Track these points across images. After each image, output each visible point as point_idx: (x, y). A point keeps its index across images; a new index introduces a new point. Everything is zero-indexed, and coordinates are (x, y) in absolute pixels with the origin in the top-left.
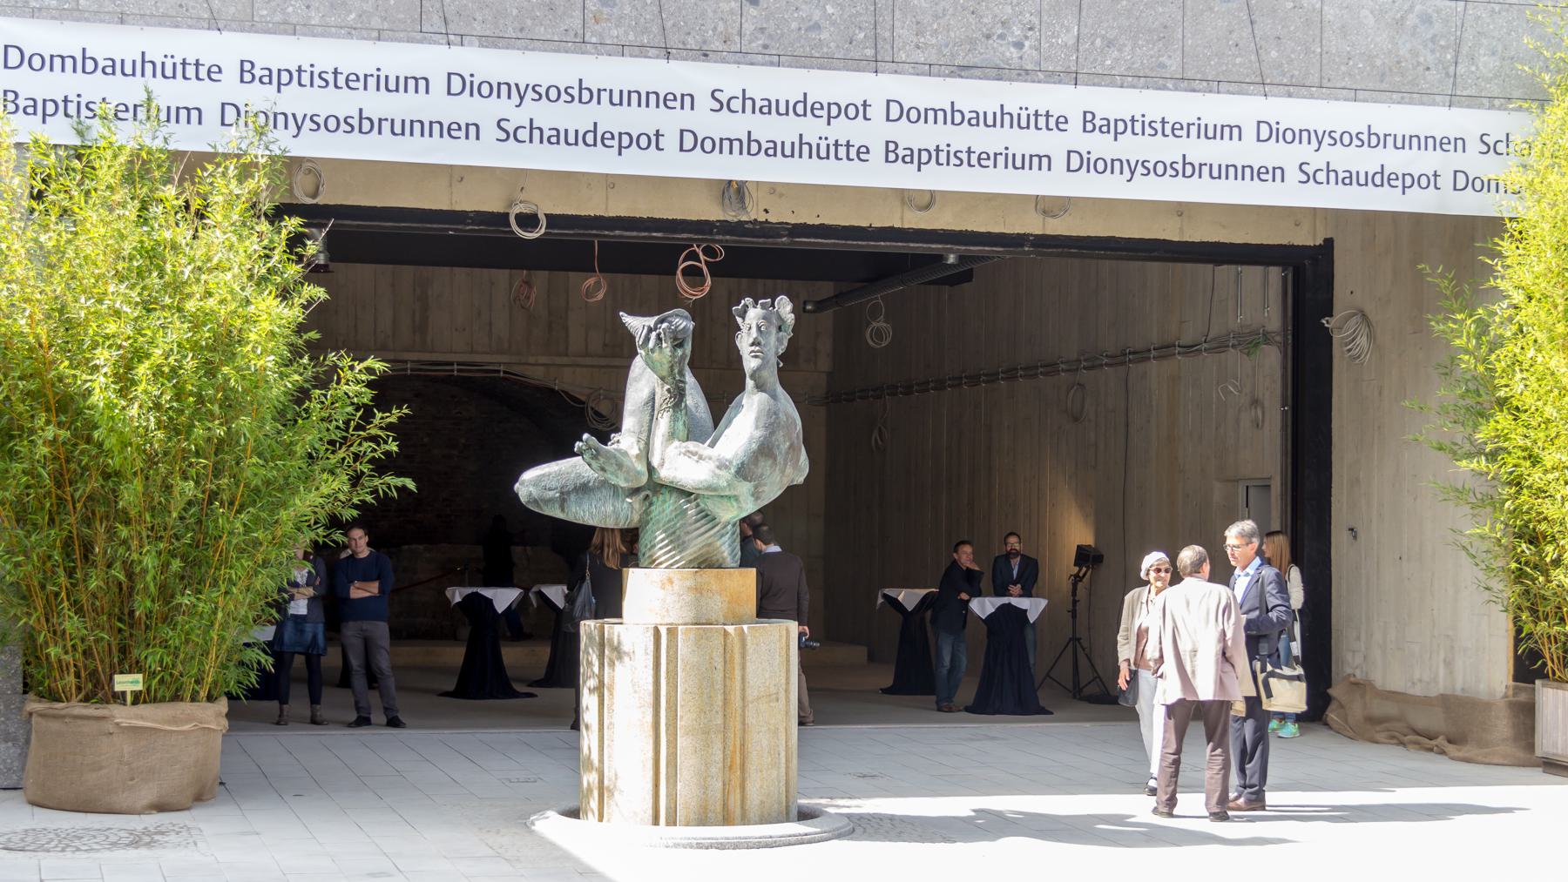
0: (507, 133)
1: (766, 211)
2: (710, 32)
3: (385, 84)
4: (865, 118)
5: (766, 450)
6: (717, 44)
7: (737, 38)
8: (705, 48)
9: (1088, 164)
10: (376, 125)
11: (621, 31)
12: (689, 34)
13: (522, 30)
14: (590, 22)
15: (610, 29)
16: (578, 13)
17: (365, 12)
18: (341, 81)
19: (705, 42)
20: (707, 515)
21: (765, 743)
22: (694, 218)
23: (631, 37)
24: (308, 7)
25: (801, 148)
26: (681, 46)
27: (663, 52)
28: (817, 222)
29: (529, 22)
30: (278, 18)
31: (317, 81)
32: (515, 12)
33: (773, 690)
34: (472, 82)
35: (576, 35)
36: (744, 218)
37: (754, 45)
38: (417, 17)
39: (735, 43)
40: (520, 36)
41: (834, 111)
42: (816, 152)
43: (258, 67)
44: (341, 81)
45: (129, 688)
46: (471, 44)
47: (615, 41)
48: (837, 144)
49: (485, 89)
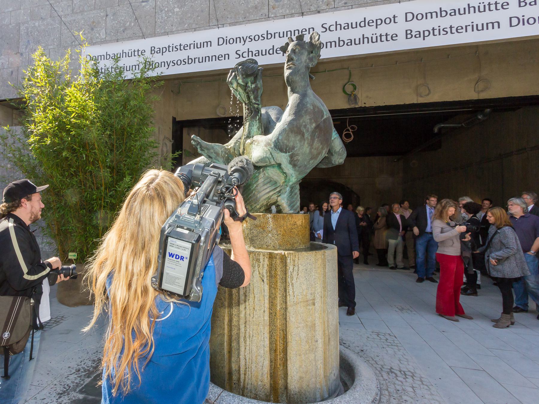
0: (239, 55)
1: (365, 103)
2: (321, 3)
3: (197, 46)
4: (395, 22)
5: (295, 129)
6: (324, 6)
7: (333, 3)
8: (319, 9)
9: (522, 21)
10: (193, 60)
11: (283, 10)
12: (312, 5)
13: (245, 18)
14: (271, 9)
15: (279, 10)
16: (266, 7)
17: (190, 23)
18: (454, 30)
19: (318, 7)
20: (271, 181)
21: (303, 335)
22: (339, 108)
23: (288, 12)
24: (172, 26)
25: (364, 39)
26: (308, 11)
27: (301, 14)
28: (384, 105)
29: (248, 14)
30: (163, 31)
31: (442, 32)
32: (242, 12)
33: (309, 297)
34: (523, 19)
35: (265, 15)
36: (357, 106)
37: (340, 4)
38: (208, 21)
39: (332, 5)
40: (244, 20)
41: (378, 23)
42: (371, 40)
43: (156, 48)
44: (454, 30)
45: (73, 258)
46: (226, 26)
47: (281, 14)
48: (381, 36)
49: (531, 21)
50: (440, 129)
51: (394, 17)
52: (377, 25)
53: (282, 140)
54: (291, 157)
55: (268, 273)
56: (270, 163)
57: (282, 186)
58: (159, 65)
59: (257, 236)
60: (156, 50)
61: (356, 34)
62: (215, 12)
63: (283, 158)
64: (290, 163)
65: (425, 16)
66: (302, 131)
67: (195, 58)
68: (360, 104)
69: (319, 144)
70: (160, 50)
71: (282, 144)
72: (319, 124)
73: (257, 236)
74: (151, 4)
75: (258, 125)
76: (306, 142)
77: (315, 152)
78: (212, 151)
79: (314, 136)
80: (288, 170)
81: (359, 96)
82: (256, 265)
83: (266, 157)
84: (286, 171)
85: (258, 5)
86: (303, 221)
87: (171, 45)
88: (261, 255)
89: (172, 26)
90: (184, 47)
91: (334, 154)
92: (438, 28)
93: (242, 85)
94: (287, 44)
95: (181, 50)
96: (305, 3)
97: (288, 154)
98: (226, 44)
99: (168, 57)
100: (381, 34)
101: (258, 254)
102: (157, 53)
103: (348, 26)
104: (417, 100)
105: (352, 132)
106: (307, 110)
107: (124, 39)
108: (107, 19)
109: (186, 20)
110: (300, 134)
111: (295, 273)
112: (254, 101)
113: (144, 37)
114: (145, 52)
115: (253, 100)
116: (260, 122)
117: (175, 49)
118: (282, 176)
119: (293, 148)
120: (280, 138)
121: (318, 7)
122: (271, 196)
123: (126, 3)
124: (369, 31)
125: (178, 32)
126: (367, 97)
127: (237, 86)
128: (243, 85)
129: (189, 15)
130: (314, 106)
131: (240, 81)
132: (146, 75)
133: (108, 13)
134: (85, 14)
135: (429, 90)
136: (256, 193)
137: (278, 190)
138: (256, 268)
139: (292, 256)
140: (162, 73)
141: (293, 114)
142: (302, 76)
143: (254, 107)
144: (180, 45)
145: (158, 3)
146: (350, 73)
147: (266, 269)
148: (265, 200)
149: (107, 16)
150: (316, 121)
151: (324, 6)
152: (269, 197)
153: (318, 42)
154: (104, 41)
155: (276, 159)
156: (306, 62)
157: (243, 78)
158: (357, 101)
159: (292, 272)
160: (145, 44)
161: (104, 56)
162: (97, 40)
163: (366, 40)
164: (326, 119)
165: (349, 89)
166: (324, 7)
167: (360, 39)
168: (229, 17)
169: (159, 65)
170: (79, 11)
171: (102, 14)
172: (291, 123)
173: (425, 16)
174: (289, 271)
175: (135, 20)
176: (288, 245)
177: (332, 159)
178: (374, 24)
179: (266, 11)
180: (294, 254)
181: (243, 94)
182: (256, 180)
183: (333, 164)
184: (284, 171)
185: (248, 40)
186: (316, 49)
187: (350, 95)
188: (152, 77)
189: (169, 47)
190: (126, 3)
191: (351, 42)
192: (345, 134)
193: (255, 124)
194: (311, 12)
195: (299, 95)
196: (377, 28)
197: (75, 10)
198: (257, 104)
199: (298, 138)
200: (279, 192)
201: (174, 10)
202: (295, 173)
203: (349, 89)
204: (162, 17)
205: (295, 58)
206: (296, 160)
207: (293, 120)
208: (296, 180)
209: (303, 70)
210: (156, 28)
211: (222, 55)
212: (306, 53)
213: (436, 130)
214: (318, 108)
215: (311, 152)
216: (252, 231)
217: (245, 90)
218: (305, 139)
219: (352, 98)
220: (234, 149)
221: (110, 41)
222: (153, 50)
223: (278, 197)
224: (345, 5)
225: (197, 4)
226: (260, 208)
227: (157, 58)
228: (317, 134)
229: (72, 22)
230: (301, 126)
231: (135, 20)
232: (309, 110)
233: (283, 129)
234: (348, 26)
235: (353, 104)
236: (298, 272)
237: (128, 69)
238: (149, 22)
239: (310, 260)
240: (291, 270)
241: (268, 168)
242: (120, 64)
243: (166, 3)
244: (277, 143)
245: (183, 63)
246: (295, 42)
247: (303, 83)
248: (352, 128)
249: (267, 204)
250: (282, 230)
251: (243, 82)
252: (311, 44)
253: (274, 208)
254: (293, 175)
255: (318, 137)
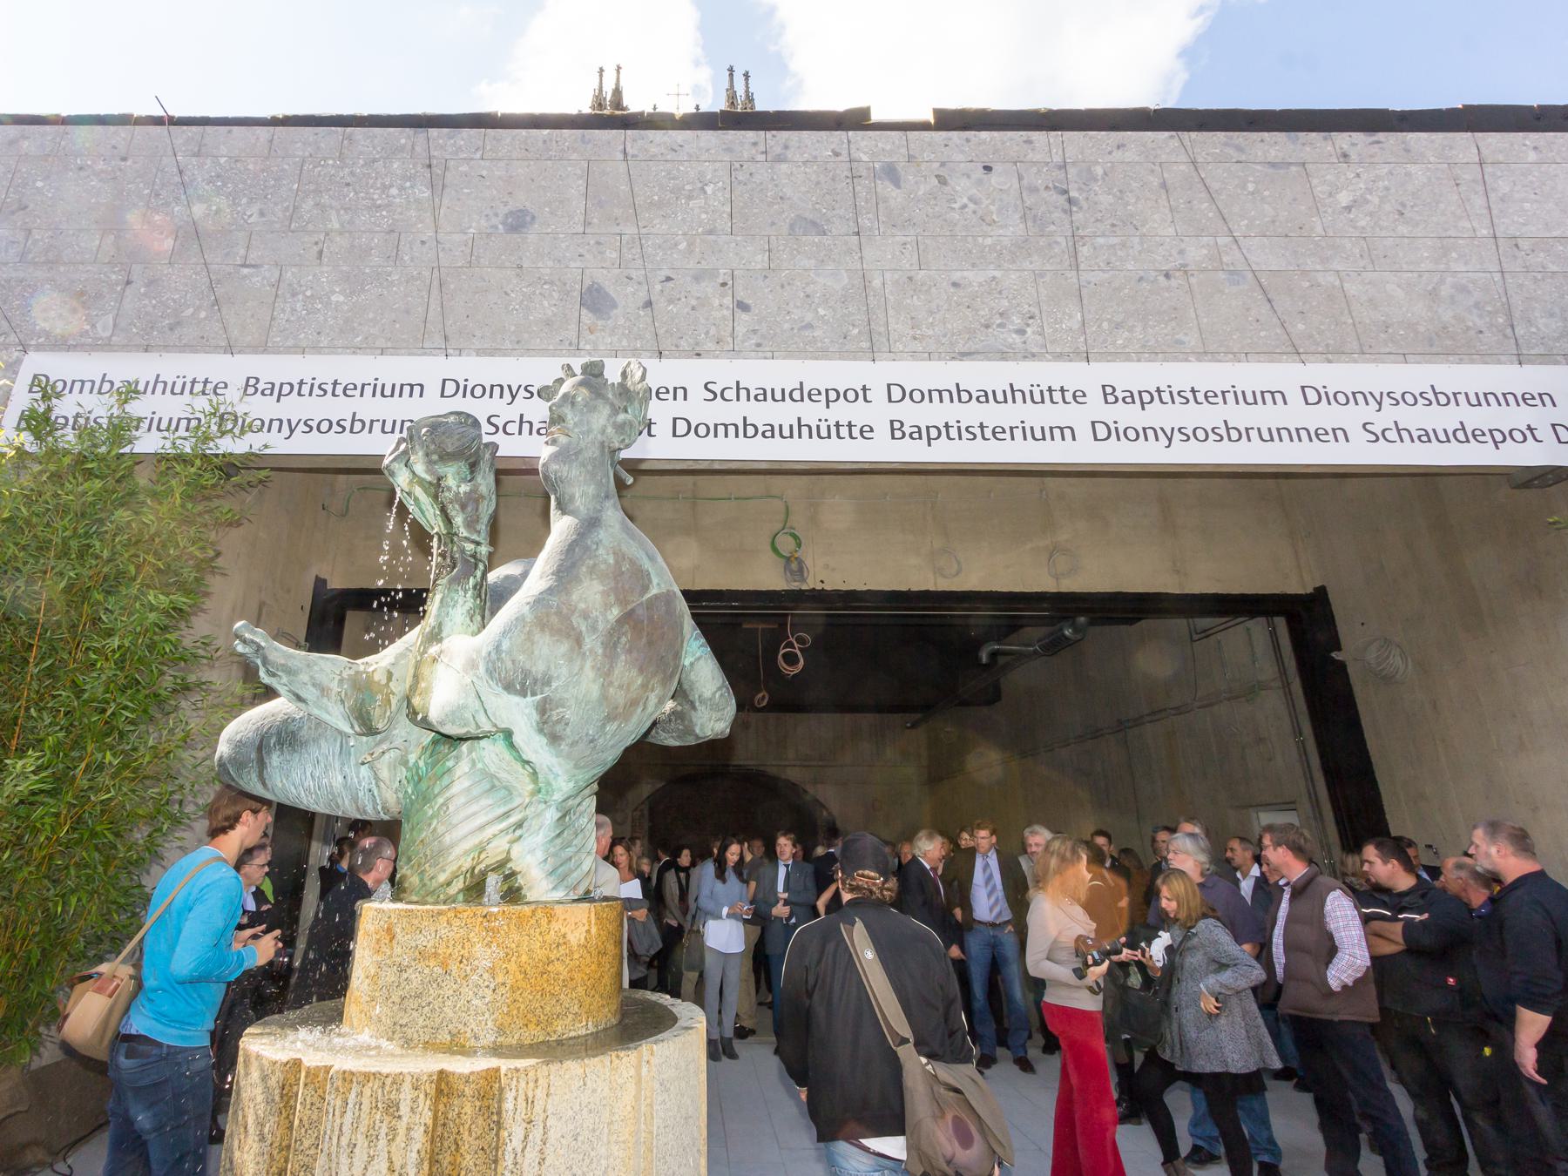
1: (822, 582)
3: (379, 391)
5: (554, 620)
9: (1115, 432)
11: (615, 339)
14: (585, 333)
19: (697, 344)
24: (319, 333)
25: (799, 428)
26: (674, 348)
27: (658, 354)
30: (290, 343)
32: (513, 328)
35: (570, 344)
36: (804, 587)
41: (831, 396)
42: (815, 432)
46: (468, 355)
50: (994, 655)
51: (864, 389)
52: (828, 401)
53: (509, 652)
54: (543, 709)
55: (426, 1166)
56: (478, 726)
57: (530, 803)
58: (264, 426)
59: (418, 996)
60: (261, 386)
61: (784, 414)
62: (441, 318)
63: (518, 713)
64: (541, 731)
65: (927, 396)
66: (574, 629)
67: (372, 421)
68: (811, 583)
69: (634, 672)
70: (272, 389)
71: (509, 665)
72: (633, 610)
73: (418, 996)
74: (267, 274)
75: (470, 604)
76: (588, 664)
77: (620, 698)
78: (304, 677)
79: (615, 646)
80: (536, 752)
81: (808, 562)
82: (384, 1130)
83: (464, 707)
84: (528, 755)
85: (554, 319)
86: (594, 930)
87: (308, 380)
88: (407, 1086)
89: (319, 333)
90: (335, 389)
91: (697, 704)
92: (956, 425)
93: (423, 479)
94: (560, 381)
95: (334, 395)
96: (667, 331)
97: (529, 699)
98: (464, 396)
99: (293, 408)
100: (837, 422)
101: (394, 1082)
102: (263, 394)
103: (763, 395)
104: (935, 584)
105: (800, 649)
106: (595, 565)
107: (167, 348)
108: (128, 292)
109: (360, 324)
110: (568, 636)
111: (531, 1155)
112: (463, 532)
113: (230, 349)
114: (226, 387)
115: (462, 529)
116: (480, 596)
117: (316, 391)
118: (521, 770)
119: (547, 681)
120: (505, 645)
121: (697, 344)
122: (489, 842)
123: (194, 260)
124: (811, 412)
125: (332, 349)
126: (827, 566)
127: (411, 482)
128: (430, 483)
129: (371, 315)
130: (620, 556)
131: (420, 469)
132: (211, 449)
133: (134, 278)
134: (62, 269)
135: (959, 563)
136: (441, 829)
137: (513, 819)
138: (382, 1143)
139: (523, 1084)
140: (266, 446)
141: (553, 574)
142: (590, 468)
143: (463, 551)
144: (335, 383)
145: (289, 274)
146: (787, 508)
147: (418, 1146)
148: (467, 853)
149: (128, 283)
150: (622, 602)
151: (710, 344)
152: (481, 843)
153: (640, 386)
154: (106, 345)
155: (494, 714)
156: (603, 432)
157: (430, 463)
158: (805, 575)
159: (519, 1150)
160: (230, 369)
161: (93, 382)
162: (83, 340)
163: (805, 430)
164: (656, 597)
165: (786, 544)
166: (710, 346)
167: (791, 426)
168: (479, 334)
169: (264, 426)
170: (43, 259)
171: (114, 277)
172: (539, 602)
173: (927, 396)
174: (509, 1148)
175: (213, 305)
176: (532, 1026)
177: (694, 720)
178: (823, 398)
179: (573, 335)
180: (531, 1074)
181: (430, 508)
182: (446, 780)
183: (697, 737)
184: (525, 757)
185: (522, 393)
186: (636, 404)
187: (788, 560)
188: (231, 454)
189: (301, 383)
190: (194, 260)
191: (771, 432)
192: (784, 655)
193: (461, 601)
194: (680, 353)
195: (577, 521)
196: (828, 407)
197: (30, 256)
198: (473, 542)
199: (564, 647)
200: (519, 825)
201: (329, 298)
202: (560, 764)
203: (786, 544)
204: (293, 310)
205: (569, 417)
206: (558, 721)
207: (550, 591)
208: (571, 785)
209: (593, 452)
210: (271, 334)
211: (355, 386)
212: (606, 411)
213: (984, 659)
214: (632, 562)
215: (604, 697)
216: (405, 976)
217: (435, 497)
218: (584, 654)
219: (794, 566)
220: (390, 675)
221: (126, 348)
222: (251, 386)
223: (512, 842)
224: (758, 349)
225: (396, 293)
226: (449, 884)
227: (260, 407)
228: (624, 639)
229: (13, 283)
230: (573, 612)
231: (213, 305)
232: (603, 567)
233: (517, 619)
234: (763, 395)
235: (795, 581)
236: (541, 1152)
237: (163, 427)
238: (253, 316)
239: (594, 1091)
240: (516, 1143)
241: (483, 743)
242: (136, 408)
243: (310, 278)
244: (494, 663)
245: (335, 428)
246: (579, 378)
247: (593, 487)
248: (801, 640)
249: (474, 868)
250: (512, 967)
251: (428, 471)
252: (624, 391)
253: (493, 882)
254: (557, 770)
255: (630, 651)
